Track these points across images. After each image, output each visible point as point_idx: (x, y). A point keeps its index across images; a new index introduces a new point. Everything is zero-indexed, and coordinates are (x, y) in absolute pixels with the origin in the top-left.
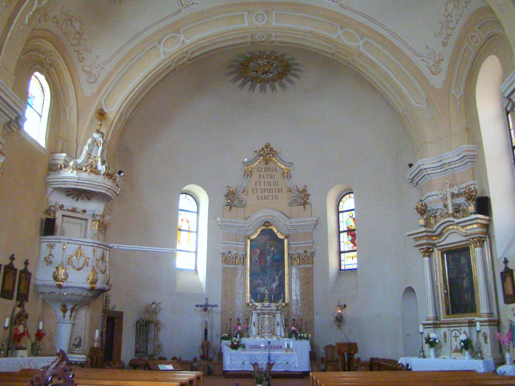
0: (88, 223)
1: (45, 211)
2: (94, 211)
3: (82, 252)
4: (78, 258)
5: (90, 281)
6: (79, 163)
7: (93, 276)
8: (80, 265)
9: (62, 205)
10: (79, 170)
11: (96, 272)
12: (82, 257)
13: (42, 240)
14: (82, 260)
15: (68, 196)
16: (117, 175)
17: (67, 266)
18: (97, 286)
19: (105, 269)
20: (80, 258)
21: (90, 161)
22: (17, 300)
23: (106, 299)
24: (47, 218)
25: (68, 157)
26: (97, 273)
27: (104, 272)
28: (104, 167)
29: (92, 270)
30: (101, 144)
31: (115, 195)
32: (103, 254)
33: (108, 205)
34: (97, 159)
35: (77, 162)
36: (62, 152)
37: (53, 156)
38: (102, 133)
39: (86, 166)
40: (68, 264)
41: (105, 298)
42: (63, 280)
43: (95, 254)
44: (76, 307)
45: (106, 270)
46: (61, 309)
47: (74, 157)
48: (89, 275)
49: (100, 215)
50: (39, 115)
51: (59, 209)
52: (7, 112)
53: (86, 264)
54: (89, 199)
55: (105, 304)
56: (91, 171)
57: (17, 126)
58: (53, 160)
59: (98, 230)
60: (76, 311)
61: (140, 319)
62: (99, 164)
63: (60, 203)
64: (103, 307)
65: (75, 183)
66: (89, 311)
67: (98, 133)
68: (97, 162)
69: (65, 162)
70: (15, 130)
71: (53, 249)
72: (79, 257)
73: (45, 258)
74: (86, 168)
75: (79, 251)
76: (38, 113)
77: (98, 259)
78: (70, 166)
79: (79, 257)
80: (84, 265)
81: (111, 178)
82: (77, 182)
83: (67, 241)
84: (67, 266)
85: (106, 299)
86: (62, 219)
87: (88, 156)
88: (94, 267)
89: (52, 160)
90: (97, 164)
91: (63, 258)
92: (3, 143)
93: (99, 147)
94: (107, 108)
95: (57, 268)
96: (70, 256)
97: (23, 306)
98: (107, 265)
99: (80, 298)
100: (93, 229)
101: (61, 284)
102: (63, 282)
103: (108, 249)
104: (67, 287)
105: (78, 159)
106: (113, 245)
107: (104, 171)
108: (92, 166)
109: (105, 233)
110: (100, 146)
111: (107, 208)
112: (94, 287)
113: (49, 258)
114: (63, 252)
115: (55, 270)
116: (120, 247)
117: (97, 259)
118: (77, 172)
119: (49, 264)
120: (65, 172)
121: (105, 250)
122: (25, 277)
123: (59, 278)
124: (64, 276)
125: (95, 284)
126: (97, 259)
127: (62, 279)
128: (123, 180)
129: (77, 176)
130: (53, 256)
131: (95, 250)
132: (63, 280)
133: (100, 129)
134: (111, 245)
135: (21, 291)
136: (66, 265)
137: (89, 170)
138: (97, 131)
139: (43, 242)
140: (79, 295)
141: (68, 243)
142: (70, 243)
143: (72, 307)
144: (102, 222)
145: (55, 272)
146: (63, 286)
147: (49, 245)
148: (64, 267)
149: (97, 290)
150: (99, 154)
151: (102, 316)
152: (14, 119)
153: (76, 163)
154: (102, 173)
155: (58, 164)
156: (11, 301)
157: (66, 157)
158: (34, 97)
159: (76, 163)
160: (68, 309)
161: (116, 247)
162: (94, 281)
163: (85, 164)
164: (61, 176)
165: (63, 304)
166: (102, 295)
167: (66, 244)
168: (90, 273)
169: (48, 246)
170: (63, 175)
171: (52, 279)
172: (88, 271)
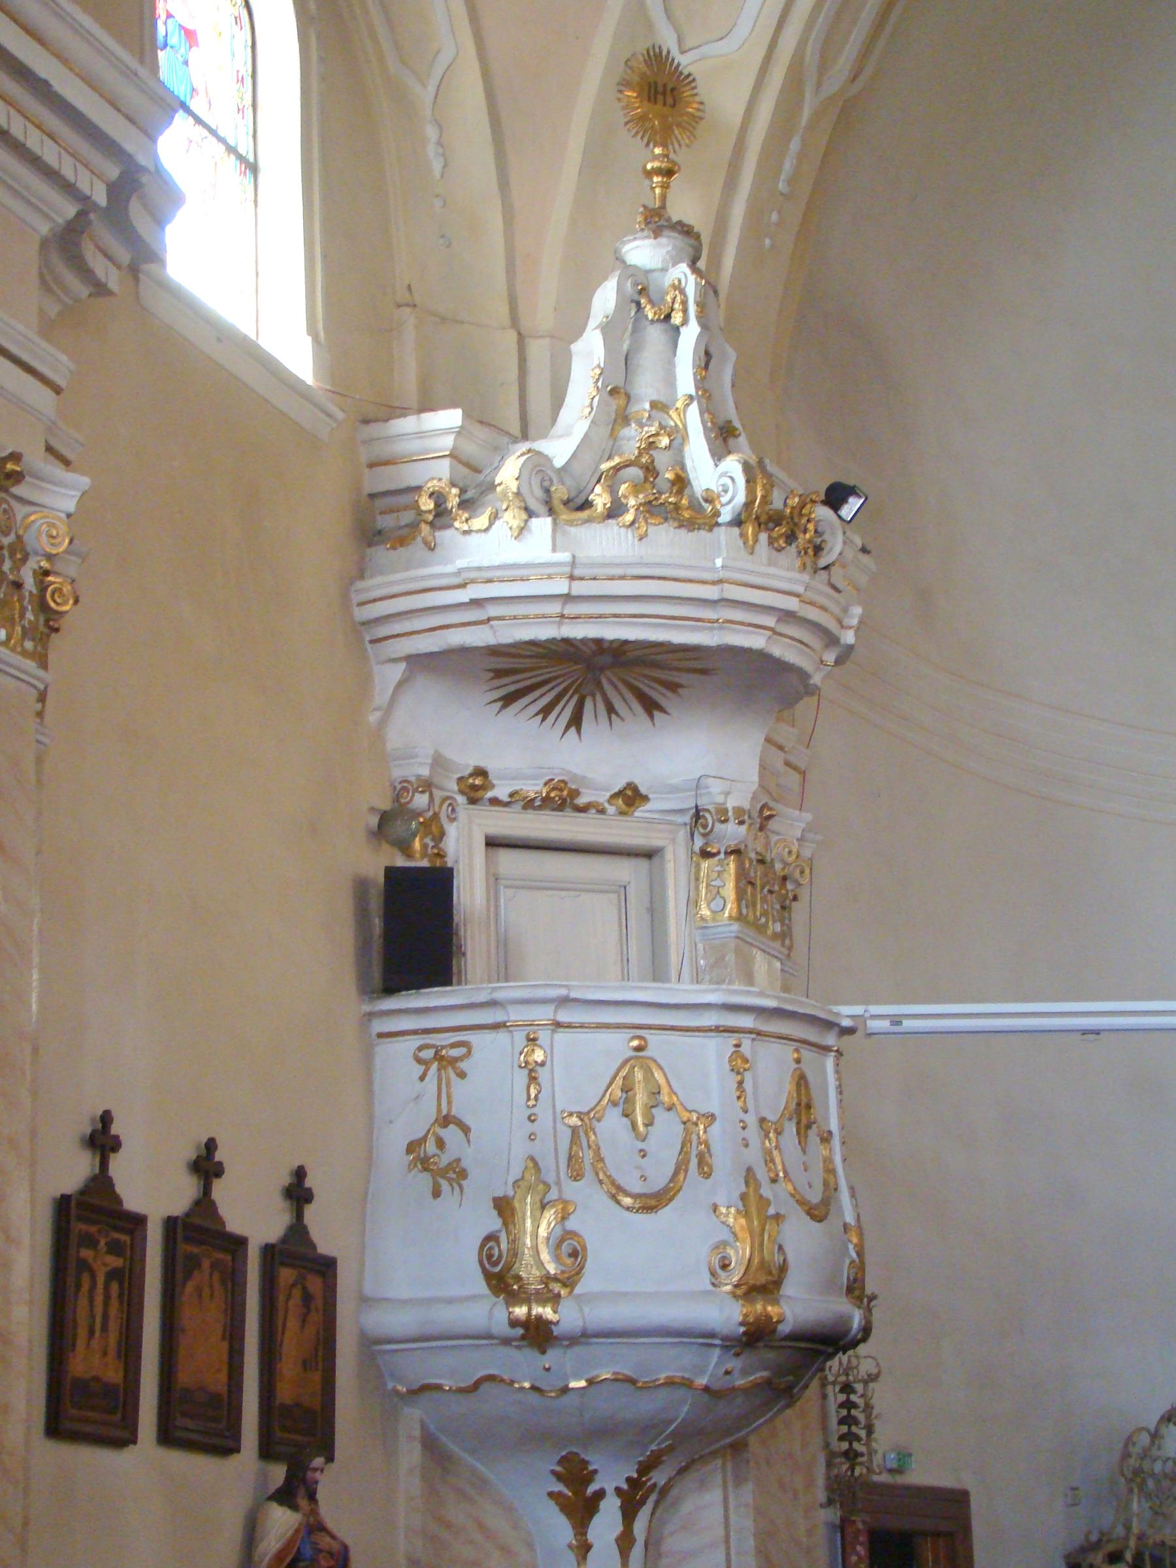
0: (663, 870)
1: (374, 821)
2: (698, 785)
3: (658, 1075)
4: (634, 1126)
5: (735, 1279)
6: (559, 463)
7: (758, 1244)
8: (659, 1179)
9: (481, 772)
10: (565, 516)
11: (771, 1211)
12: (660, 1114)
13: (379, 1026)
14: (667, 1131)
15: (508, 700)
16: (823, 512)
17: (571, 1189)
18: (789, 1316)
19: (826, 1184)
20: (649, 1124)
21: (632, 438)
22: (267, 1452)
23: (848, 1405)
24: (390, 872)
25: (482, 433)
26: (778, 1217)
27: (818, 1212)
28: (733, 465)
29: (743, 1197)
30: (692, 309)
31: (830, 657)
32: (801, 1081)
33: (787, 734)
34: (673, 419)
35: (548, 459)
36: (427, 405)
37: (369, 442)
38: (685, 230)
39: (612, 478)
40: (577, 1176)
41: (835, 1397)
42: (556, 1287)
43: (748, 1085)
44: (659, 1477)
45: (830, 1189)
46: (551, 1495)
47: (516, 429)
48: (725, 1235)
49: (739, 811)
50: (241, 158)
51: (461, 799)
52: (50, 154)
53: (694, 1162)
54: (651, 706)
55: (842, 1438)
56: (652, 509)
57: (125, 257)
58: (387, 463)
59: (740, 918)
60: (657, 1503)
61: (1094, 1538)
62: (697, 451)
63: (468, 761)
64: (829, 1465)
65: (554, 608)
66: (748, 1492)
67: (657, 233)
68: (678, 436)
69: (465, 471)
70: (112, 278)
71: (462, 1075)
72: (640, 1120)
73: (411, 1147)
74: (612, 490)
75: (639, 1075)
76: (231, 150)
77: (772, 1117)
78: (504, 494)
79: (640, 1120)
80: (681, 1167)
81: (791, 538)
82: (568, 598)
83: (544, 1014)
84: (571, 1189)
85: (848, 1405)
86: (489, 862)
87: (615, 404)
88: (749, 1175)
89: (371, 466)
90: (681, 451)
91: (532, 1137)
92: (62, 383)
93: (677, 330)
94: (689, 44)
95: (504, 1207)
96: (580, 1115)
97: (312, 1497)
98: (838, 1159)
99: (684, 1409)
100: (705, 912)
101: (539, 1318)
102: (555, 1300)
103: (830, 1039)
104: (583, 1337)
105: (544, 435)
106: (858, 1010)
107: (741, 498)
108: (650, 470)
109: (784, 936)
110: (685, 322)
111: (777, 759)
112: (769, 1317)
113: (440, 1144)
114: (533, 1092)
115: (494, 1223)
116: (908, 1024)
117: (762, 1120)
118: (555, 523)
119: (445, 1185)
120: (474, 539)
121: (807, 1054)
122: (297, 1293)
123: (528, 1272)
124: (557, 1258)
125: (776, 1302)
126: (762, 1120)
127: (547, 1279)
128: (864, 550)
129: (564, 556)
130: (466, 1130)
131: (746, 1061)
132: (556, 1287)
133: (664, 197)
134: (846, 1013)
135: (285, 1393)
136: (558, 1183)
137: (632, 502)
138: (647, 222)
139: (381, 1035)
140: (670, 1383)
141: (558, 1025)
142: (569, 1026)
143: (629, 1480)
144: (761, 861)
145: (491, 1238)
146: (556, 1331)
147: (428, 1054)
148: (553, 1195)
149: (794, 1337)
150: (686, 383)
151: (831, 1526)
152: (100, 197)
153: (538, 464)
154: (726, 515)
155: (418, 489)
156: (234, 1460)
157: (460, 432)
158: (190, 36)
159: (538, 464)
160: (600, 1494)
161: (884, 1025)
162: (762, 1279)
163: (605, 466)
164: (449, 569)
165: (563, 1461)
166: (815, 1384)
167: (544, 1036)
168: (731, 1220)
169: (419, 1061)
170: (461, 563)
171: (481, 1287)
172: (715, 1208)
